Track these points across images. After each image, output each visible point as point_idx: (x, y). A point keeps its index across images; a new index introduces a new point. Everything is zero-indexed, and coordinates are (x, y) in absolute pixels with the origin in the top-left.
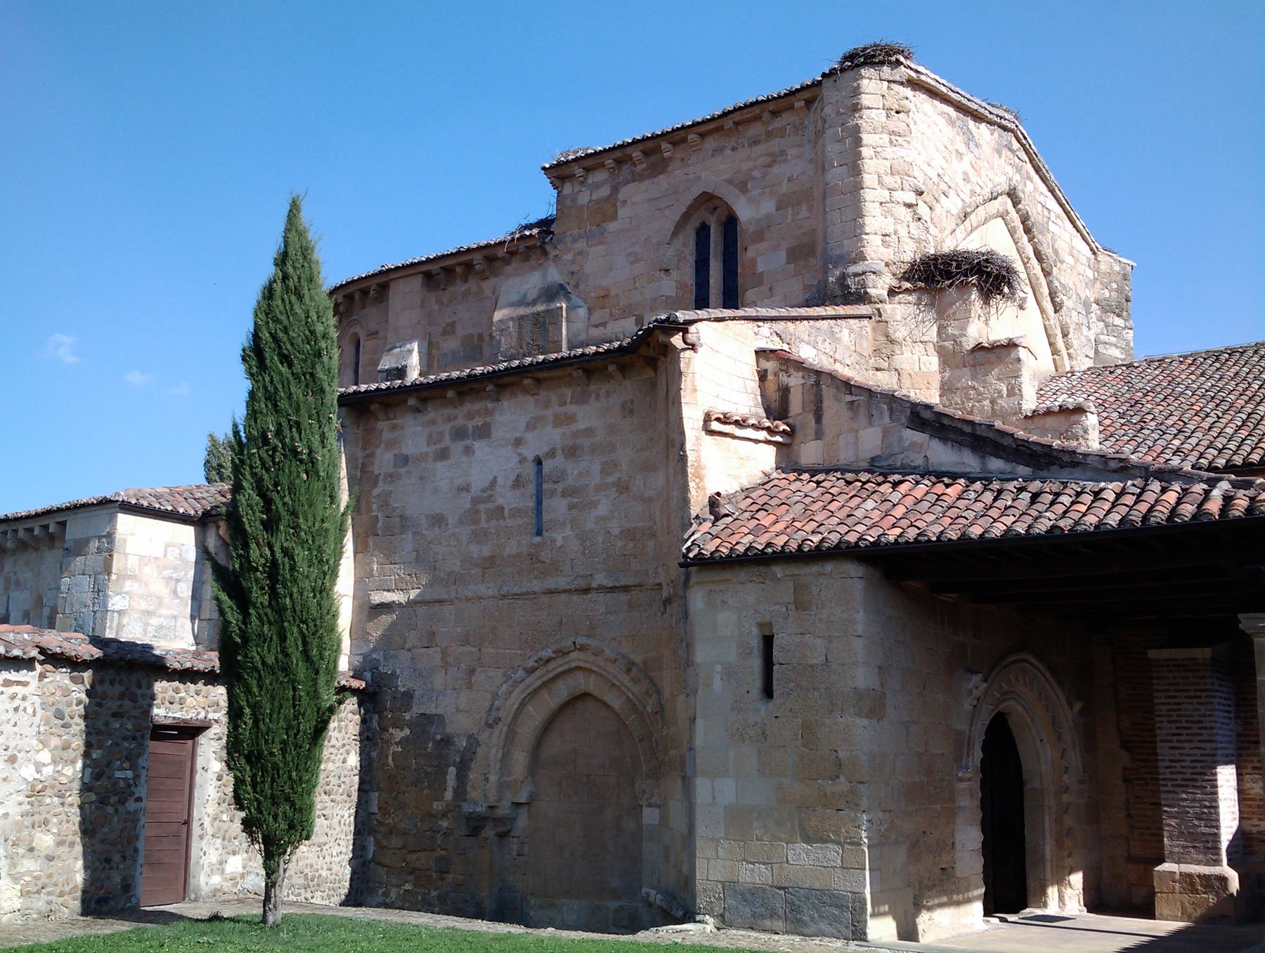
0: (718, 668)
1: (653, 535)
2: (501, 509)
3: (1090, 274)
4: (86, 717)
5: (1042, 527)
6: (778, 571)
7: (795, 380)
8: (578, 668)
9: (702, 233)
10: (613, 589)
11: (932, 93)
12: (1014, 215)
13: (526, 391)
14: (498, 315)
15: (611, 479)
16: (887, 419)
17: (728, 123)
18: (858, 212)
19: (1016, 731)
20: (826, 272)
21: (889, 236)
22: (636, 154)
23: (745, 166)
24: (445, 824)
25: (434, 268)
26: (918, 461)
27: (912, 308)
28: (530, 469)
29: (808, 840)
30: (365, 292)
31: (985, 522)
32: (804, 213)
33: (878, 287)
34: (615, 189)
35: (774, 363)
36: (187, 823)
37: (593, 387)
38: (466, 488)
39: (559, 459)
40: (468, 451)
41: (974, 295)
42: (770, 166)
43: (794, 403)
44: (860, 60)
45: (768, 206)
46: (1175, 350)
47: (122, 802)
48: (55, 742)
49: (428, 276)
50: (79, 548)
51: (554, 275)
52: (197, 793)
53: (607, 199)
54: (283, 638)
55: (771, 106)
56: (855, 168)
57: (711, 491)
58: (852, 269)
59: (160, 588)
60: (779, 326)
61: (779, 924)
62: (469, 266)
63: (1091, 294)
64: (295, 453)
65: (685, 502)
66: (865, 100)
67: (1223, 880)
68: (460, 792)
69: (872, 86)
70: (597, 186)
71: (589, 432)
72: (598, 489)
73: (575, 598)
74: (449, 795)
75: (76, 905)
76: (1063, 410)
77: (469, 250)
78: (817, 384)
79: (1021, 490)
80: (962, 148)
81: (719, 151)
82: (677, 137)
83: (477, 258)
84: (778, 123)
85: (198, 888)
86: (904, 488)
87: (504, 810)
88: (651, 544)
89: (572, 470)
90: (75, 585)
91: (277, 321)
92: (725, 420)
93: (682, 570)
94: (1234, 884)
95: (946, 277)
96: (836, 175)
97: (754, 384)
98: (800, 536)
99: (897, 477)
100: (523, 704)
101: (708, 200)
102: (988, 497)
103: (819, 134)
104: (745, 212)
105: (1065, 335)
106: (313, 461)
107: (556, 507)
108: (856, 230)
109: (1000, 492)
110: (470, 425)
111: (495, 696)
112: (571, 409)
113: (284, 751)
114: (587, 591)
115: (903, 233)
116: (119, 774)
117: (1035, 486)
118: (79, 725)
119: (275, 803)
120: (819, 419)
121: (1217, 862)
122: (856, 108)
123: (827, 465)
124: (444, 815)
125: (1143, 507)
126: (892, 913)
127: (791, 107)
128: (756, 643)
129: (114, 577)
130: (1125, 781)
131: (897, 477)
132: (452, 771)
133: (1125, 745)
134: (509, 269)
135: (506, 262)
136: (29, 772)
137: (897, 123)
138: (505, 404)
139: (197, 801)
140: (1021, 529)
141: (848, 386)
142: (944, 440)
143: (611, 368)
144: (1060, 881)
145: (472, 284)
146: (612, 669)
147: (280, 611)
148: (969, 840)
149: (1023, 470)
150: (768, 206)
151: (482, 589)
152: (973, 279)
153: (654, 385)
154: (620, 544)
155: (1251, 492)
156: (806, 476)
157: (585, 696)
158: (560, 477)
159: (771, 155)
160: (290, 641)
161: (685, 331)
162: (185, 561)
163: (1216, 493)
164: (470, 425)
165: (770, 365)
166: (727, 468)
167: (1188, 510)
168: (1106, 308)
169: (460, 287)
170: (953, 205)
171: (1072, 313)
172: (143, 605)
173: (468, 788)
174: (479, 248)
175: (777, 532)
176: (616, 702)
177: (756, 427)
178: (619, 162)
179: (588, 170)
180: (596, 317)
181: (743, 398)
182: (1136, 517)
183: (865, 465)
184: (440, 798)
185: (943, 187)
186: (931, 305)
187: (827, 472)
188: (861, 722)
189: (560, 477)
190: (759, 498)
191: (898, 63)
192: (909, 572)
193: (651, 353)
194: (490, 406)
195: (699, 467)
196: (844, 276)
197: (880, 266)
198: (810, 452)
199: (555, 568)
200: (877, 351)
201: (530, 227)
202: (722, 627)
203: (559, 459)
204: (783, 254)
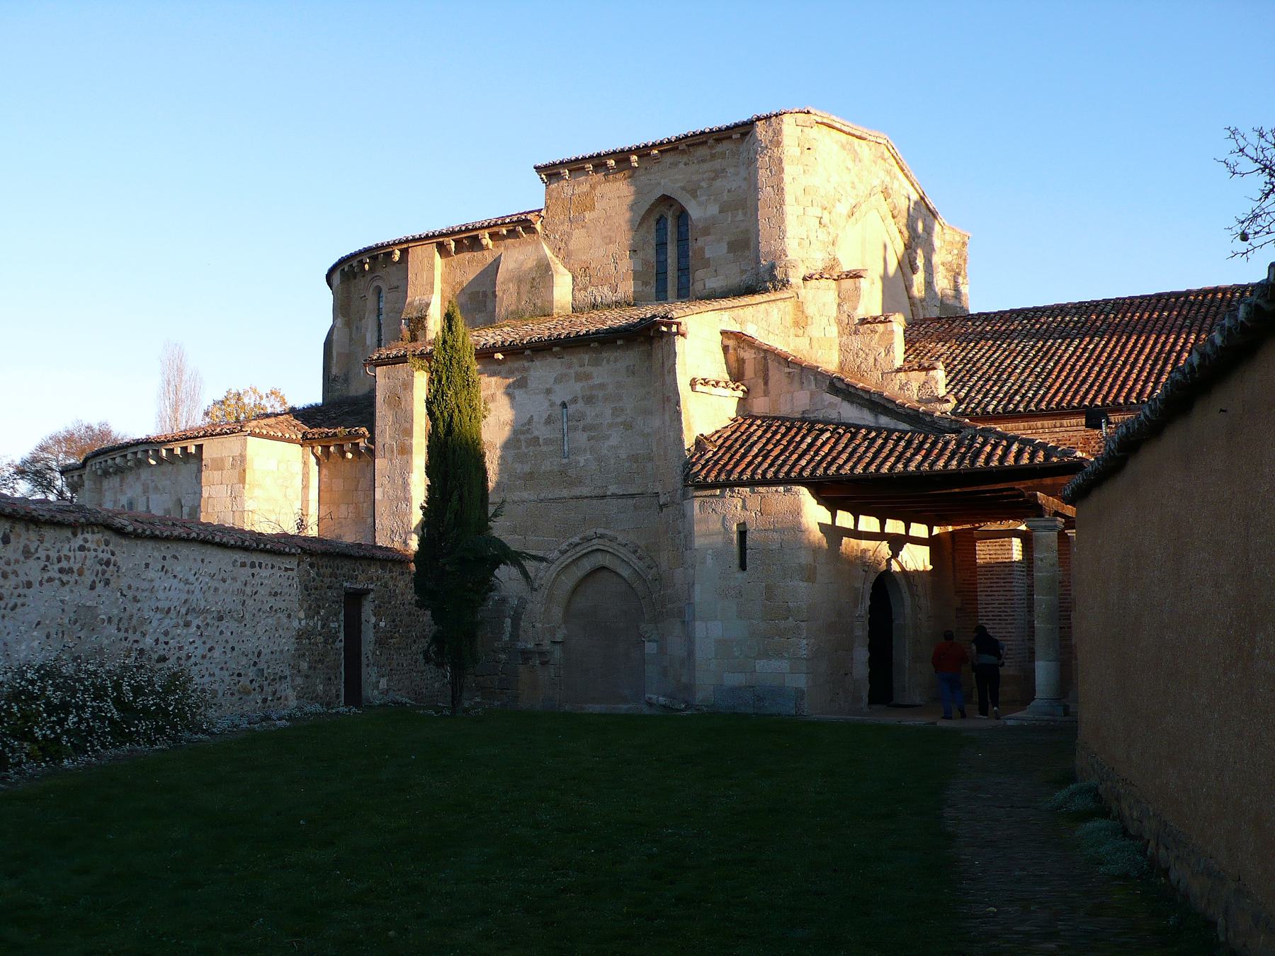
0: (710, 551)
1: (651, 459)
7: (748, 355)
8: (598, 550)
9: (661, 221)
15: (619, 420)
16: (813, 386)
23: (695, 178)
32: (740, 217)
35: (735, 342)
37: (604, 355)
39: (580, 405)
42: (714, 179)
43: (748, 362)
45: (713, 209)
47: (334, 642)
53: (587, 194)
72: (611, 426)
74: (506, 637)
80: (850, 164)
81: (676, 164)
84: (720, 148)
88: (649, 465)
89: (590, 412)
92: (705, 382)
100: (558, 575)
101: (666, 200)
104: (695, 212)
112: (588, 369)
114: (603, 497)
116: (332, 625)
120: (766, 383)
129: (247, 486)
132: (508, 621)
136: (295, 624)
138: (537, 363)
142: (852, 402)
143: (619, 342)
146: (622, 550)
150: (713, 209)
151: (525, 495)
153: (650, 355)
154: (627, 465)
157: (603, 568)
158: (582, 416)
159: (715, 171)
165: (731, 343)
170: (843, 208)
173: (521, 633)
176: (625, 573)
181: (716, 368)
185: (838, 196)
189: (582, 416)
194: (526, 364)
199: (580, 482)
203: (580, 405)
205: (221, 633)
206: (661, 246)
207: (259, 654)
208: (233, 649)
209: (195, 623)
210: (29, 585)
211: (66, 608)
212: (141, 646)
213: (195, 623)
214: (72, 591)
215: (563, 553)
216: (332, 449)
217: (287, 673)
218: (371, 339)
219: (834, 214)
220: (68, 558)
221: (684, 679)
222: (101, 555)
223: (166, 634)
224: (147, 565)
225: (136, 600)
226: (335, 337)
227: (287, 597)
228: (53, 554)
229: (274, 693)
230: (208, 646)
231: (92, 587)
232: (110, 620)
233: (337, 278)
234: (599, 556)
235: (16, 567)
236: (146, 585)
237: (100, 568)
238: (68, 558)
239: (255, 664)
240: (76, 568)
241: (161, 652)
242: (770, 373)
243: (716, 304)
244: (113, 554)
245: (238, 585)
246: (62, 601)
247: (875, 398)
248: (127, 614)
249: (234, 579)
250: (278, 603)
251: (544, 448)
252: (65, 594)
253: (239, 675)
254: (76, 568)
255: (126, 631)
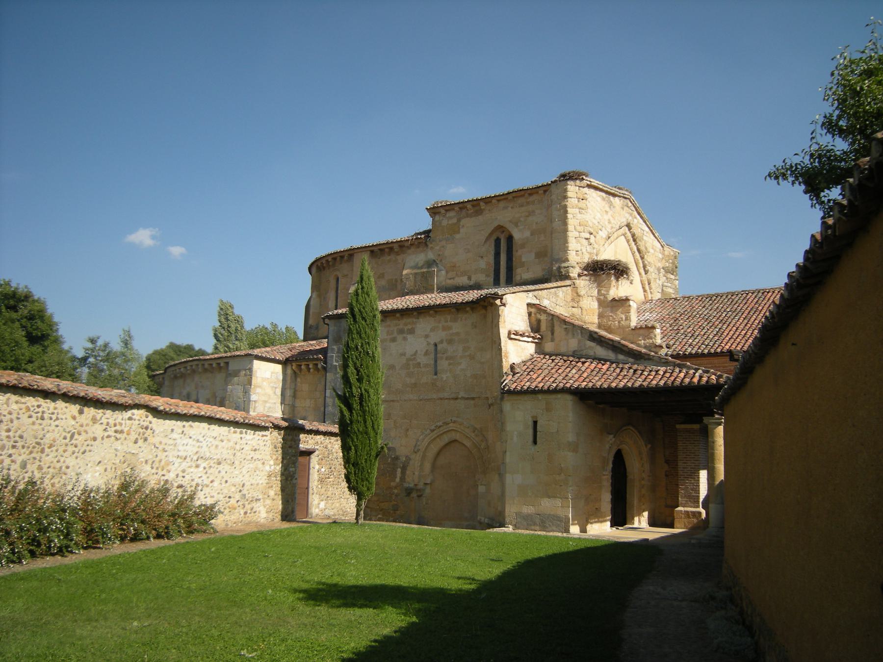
2: (419, 364)
3: (660, 256)
4: (282, 448)
5: (637, 385)
6: (540, 396)
7: (543, 317)
9: (498, 242)
10: (468, 399)
11: (596, 188)
12: (629, 234)
13: (431, 316)
14: (405, 272)
15: (467, 354)
16: (580, 336)
17: (510, 197)
18: (565, 241)
19: (625, 456)
20: (552, 265)
21: (578, 252)
22: (469, 206)
24: (396, 491)
25: (375, 249)
26: (591, 353)
27: (587, 282)
28: (432, 348)
29: (549, 497)
30: (342, 257)
31: (617, 381)
33: (574, 273)
34: (459, 220)
35: (535, 310)
36: (308, 488)
38: (404, 354)
39: (445, 345)
40: (405, 339)
41: (613, 278)
43: (543, 325)
44: (566, 177)
45: (527, 234)
46: (694, 293)
48: (274, 457)
49: (372, 252)
50: (236, 374)
51: (431, 256)
52: (311, 477)
54: (365, 422)
55: (529, 192)
56: (565, 224)
57: (511, 363)
58: (563, 265)
59: (269, 391)
60: (536, 293)
61: (538, 528)
62: (391, 249)
63: (660, 265)
64: (368, 353)
65: (501, 367)
66: (569, 194)
67: (700, 513)
68: (403, 479)
69: (572, 188)
70: (451, 218)
71: (458, 334)
73: (452, 402)
74: (398, 480)
75: (280, 517)
76: (647, 327)
77: (392, 242)
78: (552, 319)
79: (630, 368)
80: (608, 209)
81: (505, 208)
82: (487, 200)
83: (396, 246)
84: (531, 199)
85: (312, 514)
86: (587, 364)
87: (421, 486)
90: (234, 389)
91: (360, 304)
92: (516, 334)
93: (497, 394)
94: (704, 515)
95: (602, 270)
96: (557, 224)
97: (526, 318)
98: (548, 384)
99: (583, 360)
100: (429, 444)
101: (500, 228)
102: (618, 370)
103: (549, 206)
104: (517, 235)
105: (649, 284)
106: (374, 357)
107: (443, 364)
108: (565, 249)
109: (622, 368)
110: (406, 328)
111: (418, 440)
112: (450, 324)
113: (366, 462)
114: (456, 399)
115: (584, 251)
117: (635, 367)
118: (280, 451)
119: (362, 481)
120: (553, 334)
121: (698, 507)
122: (565, 197)
123: (556, 352)
124: (396, 488)
125: (672, 378)
126: (578, 524)
127: (537, 193)
128: (531, 423)
130: (666, 476)
131: (583, 360)
132: (399, 470)
133: (667, 462)
134: (410, 251)
135: (409, 248)
136: (267, 468)
137: (582, 204)
139: (311, 480)
140: (630, 385)
141: (564, 322)
142: (602, 346)
144: (639, 514)
145: (393, 257)
147: (364, 412)
148: (606, 498)
149: (631, 360)
152: (612, 272)
153: (485, 316)
155: (708, 375)
156: (547, 357)
157: (456, 441)
160: (368, 423)
161: (502, 299)
162: (277, 378)
163: (697, 374)
164: (406, 328)
165: (533, 310)
166: (517, 352)
167: (687, 380)
168: (667, 271)
169: (387, 258)
170: (603, 234)
171: (652, 275)
172: (264, 398)
174: (397, 242)
175: (538, 383)
176: (468, 444)
177: (528, 337)
178: (460, 208)
179: (446, 211)
180: (450, 275)
182: (670, 382)
183: (571, 353)
184: (394, 481)
185: (600, 227)
186: (595, 281)
187: (556, 355)
188: (570, 454)
190: (529, 365)
191: (583, 179)
192: (587, 397)
193: (486, 304)
195: (507, 353)
196: (559, 268)
197: (575, 264)
198: (549, 347)
200: (573, 300)
201: (420, 234)
202: (517, 418)
203: (445, 345)
204: (533, 255)
205: (219, 472)
206: (497, 255)
207: (243, 485)
208: (226, 482)
209: (203, 465)
210: (95, 439)
211: (118, 454)
212: (165, 478)
213: (203, 465)
214: (122, 444)
215: (432, 431)
216: (303, 367)
217: (260, 497)
218: (332, 304)
219: (598, 237)
220: (121, 424)
221: (499, 508)
222: (142, 423)
223: (184, 471)
224: (172, 430)
225: (164, 450)
226: (312, 303)
227: (263, 452)
228: (111, 422)
229: (252, 509)
230: (210, 480)
231: (136, 442)
232: (146, 462)
233: (314, 270)
234: (453, 433)
235: (87, 428)
236: (171, 442)
237: (142, 431)
238: (121, 424)
239: (240, 491)
240: (126, 430)
241: (180, 482)
242: (556, 328)
243: (525, 288)
244: (150, 423)
245: (231, 444)
246: (116, 450)
247: (616, 344)
248: (158, 459)
249: (229, 440)
250: (257, 455)
251: (423, 370)
252: (118, 445)
253: (230, 497)
254: (126, 430)
255: (157, 468)
